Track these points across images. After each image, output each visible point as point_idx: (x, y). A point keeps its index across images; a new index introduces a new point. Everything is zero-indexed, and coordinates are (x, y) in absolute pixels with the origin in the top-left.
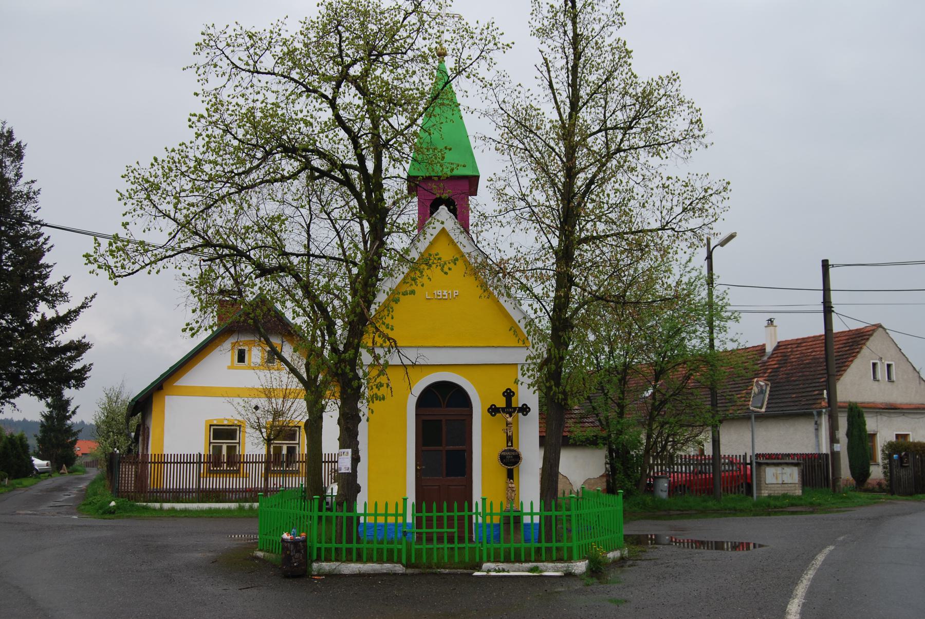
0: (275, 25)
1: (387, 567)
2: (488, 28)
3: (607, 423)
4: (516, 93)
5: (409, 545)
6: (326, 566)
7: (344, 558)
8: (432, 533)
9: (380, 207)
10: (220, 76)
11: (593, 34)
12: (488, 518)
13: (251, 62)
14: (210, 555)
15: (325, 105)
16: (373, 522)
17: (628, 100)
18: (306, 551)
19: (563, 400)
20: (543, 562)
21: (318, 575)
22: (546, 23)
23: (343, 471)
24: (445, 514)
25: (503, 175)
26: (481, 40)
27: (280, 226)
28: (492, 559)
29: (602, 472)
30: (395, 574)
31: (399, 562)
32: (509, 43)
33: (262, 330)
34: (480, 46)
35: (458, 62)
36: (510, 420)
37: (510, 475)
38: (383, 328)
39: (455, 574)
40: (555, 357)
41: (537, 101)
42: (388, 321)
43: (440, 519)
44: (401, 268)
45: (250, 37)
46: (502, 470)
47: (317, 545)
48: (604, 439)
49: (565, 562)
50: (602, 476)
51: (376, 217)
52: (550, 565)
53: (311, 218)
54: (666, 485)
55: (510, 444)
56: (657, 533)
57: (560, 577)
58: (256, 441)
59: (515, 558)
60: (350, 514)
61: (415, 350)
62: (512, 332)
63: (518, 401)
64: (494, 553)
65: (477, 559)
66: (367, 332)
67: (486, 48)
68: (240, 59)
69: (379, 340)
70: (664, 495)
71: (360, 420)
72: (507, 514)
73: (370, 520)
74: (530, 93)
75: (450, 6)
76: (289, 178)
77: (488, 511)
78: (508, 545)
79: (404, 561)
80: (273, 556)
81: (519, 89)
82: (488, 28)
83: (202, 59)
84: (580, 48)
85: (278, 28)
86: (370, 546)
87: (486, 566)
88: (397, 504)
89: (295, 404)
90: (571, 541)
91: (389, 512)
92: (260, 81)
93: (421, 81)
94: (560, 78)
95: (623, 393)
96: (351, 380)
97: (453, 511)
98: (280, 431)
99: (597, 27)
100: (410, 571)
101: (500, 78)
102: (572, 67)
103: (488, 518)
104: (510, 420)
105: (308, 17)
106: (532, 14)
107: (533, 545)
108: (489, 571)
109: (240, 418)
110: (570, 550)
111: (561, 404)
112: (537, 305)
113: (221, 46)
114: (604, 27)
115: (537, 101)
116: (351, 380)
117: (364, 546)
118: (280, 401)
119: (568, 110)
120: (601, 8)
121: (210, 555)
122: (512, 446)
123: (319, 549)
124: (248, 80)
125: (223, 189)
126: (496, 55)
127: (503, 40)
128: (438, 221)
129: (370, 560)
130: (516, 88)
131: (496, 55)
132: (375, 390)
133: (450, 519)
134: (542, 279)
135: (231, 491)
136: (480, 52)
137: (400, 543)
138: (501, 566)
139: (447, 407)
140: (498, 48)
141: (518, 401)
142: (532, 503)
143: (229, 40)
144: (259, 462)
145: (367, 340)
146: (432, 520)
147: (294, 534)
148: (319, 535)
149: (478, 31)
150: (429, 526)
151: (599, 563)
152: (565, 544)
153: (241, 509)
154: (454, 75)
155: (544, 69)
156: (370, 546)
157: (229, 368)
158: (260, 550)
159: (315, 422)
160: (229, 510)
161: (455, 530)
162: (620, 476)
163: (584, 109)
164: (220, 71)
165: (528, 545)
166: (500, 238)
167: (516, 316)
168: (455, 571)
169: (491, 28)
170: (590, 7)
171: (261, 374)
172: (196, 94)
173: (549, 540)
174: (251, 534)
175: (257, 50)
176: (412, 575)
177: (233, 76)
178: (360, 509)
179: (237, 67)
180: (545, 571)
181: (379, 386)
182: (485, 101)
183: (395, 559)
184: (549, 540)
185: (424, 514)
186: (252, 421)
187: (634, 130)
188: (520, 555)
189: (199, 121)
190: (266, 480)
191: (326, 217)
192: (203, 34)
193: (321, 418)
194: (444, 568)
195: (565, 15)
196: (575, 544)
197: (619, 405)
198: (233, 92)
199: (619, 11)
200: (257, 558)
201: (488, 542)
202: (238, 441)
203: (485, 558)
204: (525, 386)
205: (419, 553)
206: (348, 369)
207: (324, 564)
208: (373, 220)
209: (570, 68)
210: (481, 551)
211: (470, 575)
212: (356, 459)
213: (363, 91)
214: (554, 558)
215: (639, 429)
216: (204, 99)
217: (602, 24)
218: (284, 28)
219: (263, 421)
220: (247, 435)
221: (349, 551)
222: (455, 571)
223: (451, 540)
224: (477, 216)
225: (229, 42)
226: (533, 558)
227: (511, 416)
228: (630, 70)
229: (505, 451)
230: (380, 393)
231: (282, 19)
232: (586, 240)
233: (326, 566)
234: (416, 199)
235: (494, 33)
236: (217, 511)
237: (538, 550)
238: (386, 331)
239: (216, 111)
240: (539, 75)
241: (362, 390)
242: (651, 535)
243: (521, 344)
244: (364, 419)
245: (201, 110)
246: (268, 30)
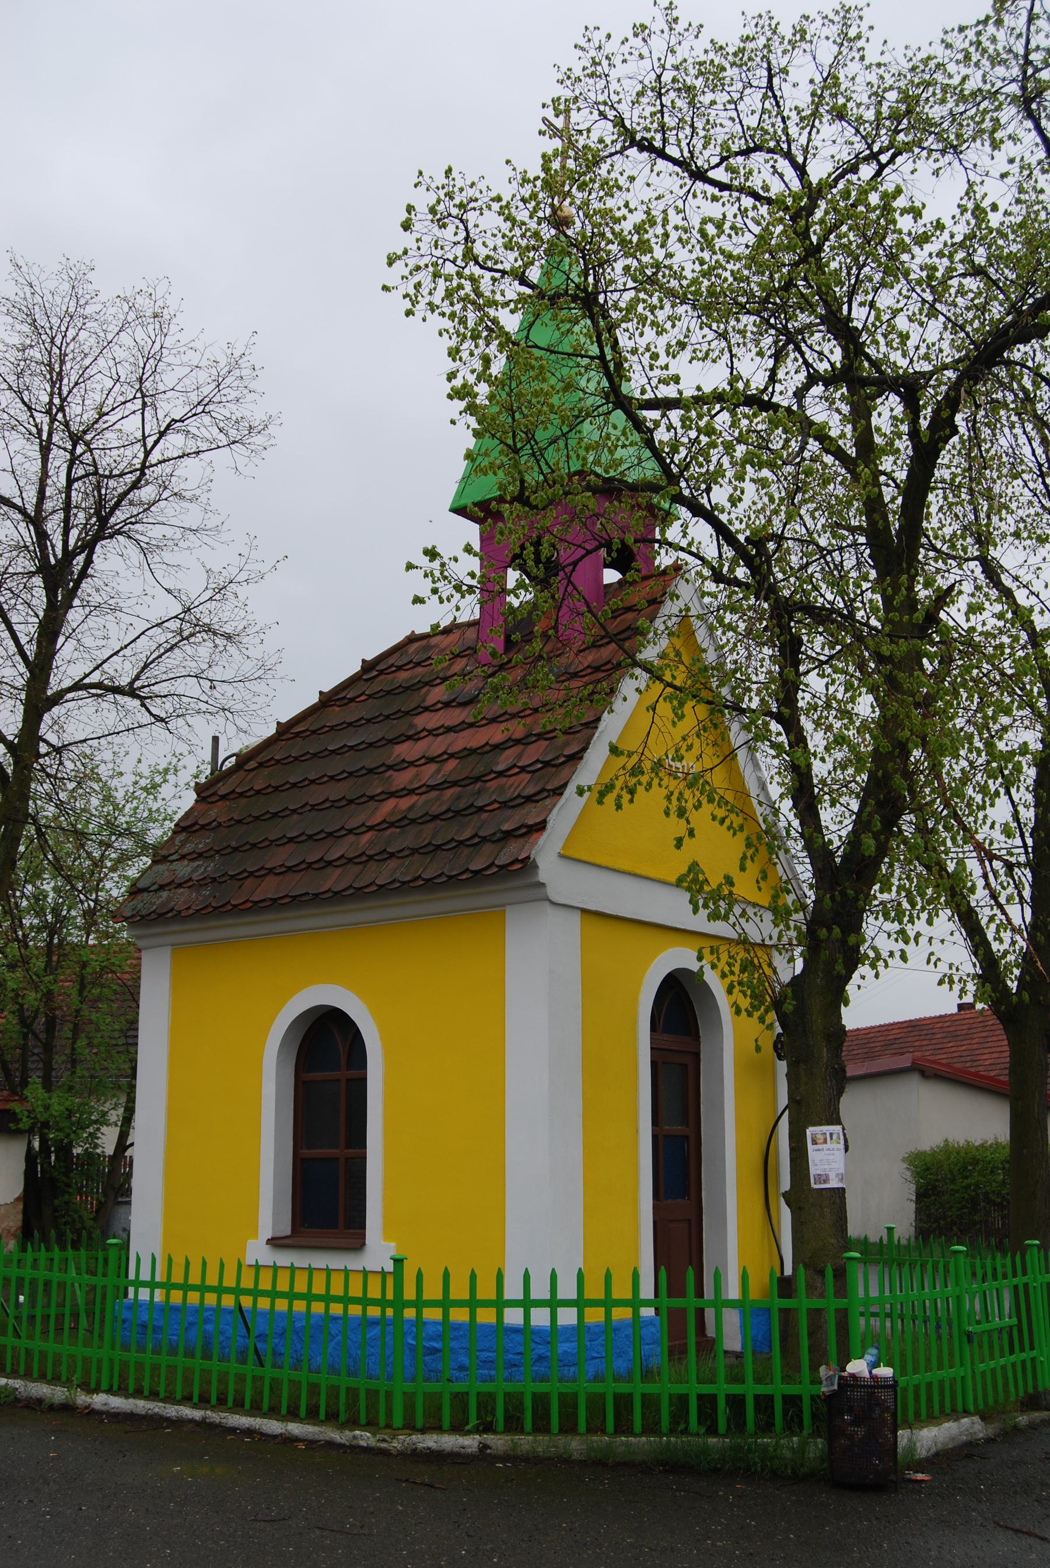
16: (574, 1321)
60: (677, 1303)
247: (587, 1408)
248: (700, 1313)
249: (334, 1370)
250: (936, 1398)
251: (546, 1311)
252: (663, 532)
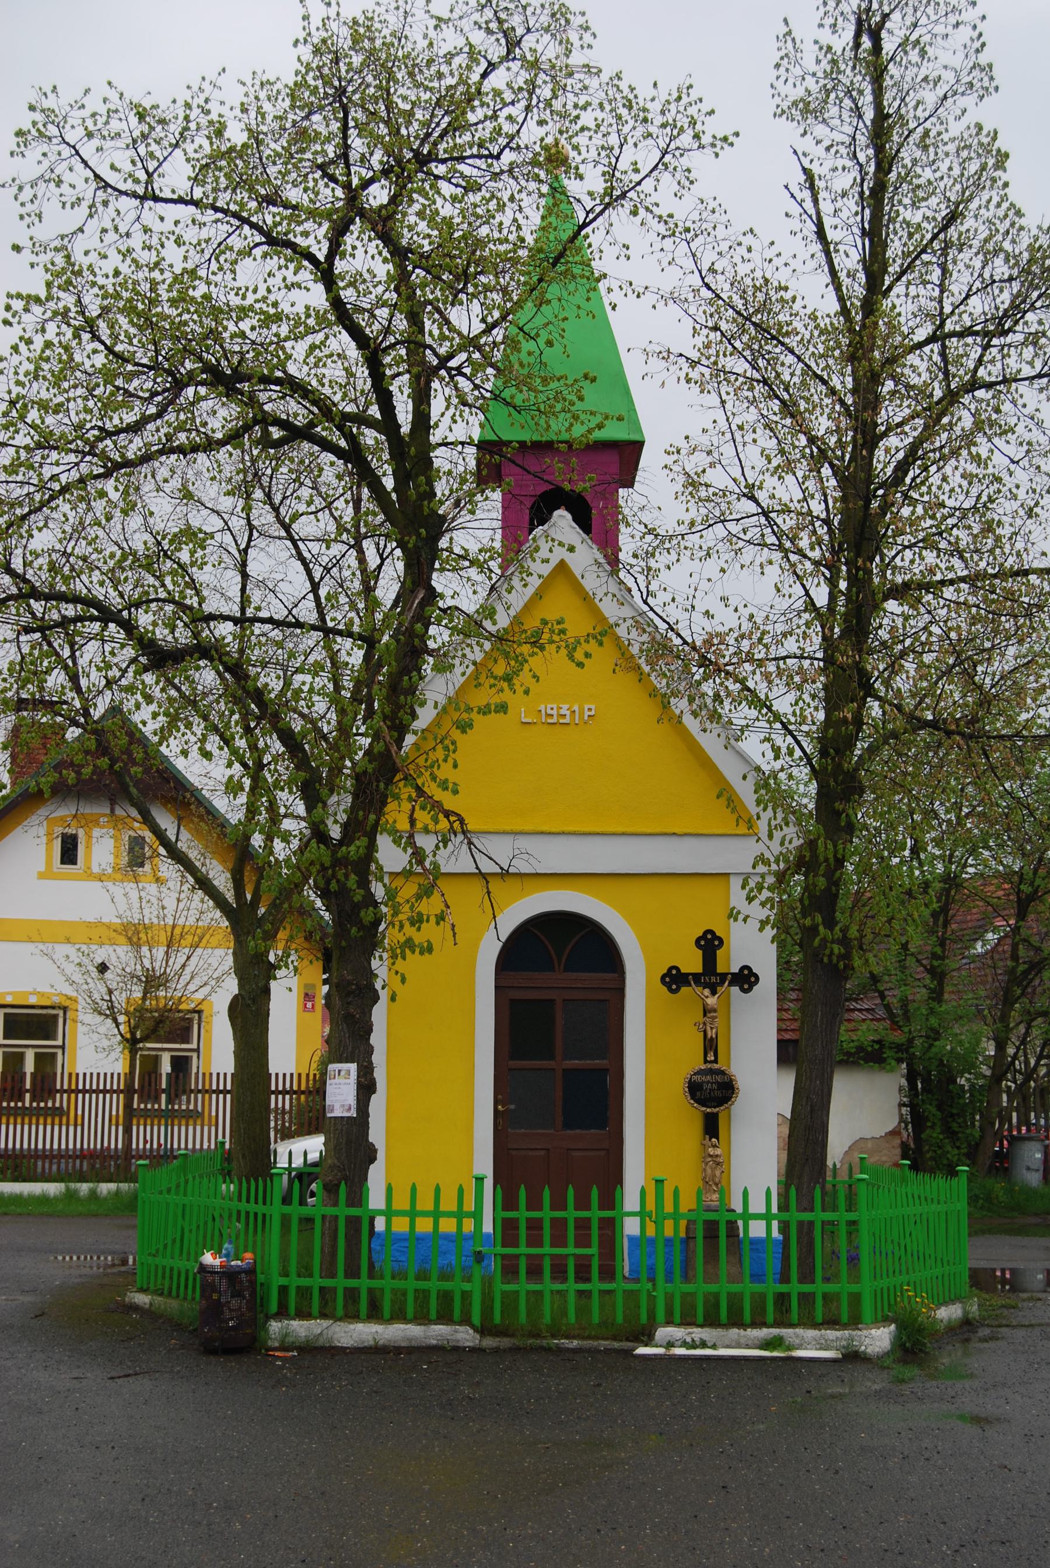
0: (195, 88)
1: (438, 1332)
2: (679, 98)
3: (906, 1012)
4: (742, 251)
5: (487, 1284)
6: (300, 1328)
7: (340, 1312)
8: (541, 1257)
9: (426, 511)
10: (68, 206)
11: (919, 112)
12: (669, 1225)
13: (142, 176)
14: (27, 1299)
15: (306, 275)
16: (763, 1234)
17: (1000, 268)
18: (253, 1293)
19: (841, 957)
20: (791, 1325)
21: (283, 1348)
22: (814, 88)
23: (338, 1113)
24: (571, 1214)
25: (704, 441)
26: (664, 126)
27: (192, 553)
28: (677, 1318)
29: (892, 1123)
30: (456, 1349)
31: (466, 1321)
32: (729, 133)
33: (134, 791)
34: (660, 141)
35: (610, 175)
36: (711, 1001)
37: (711, 1128)
38: (432, 790)
39: (593, 1352)
40: (826, 860)
41: (789, 269)
42: (445, 772)
43: (559, 1225)
44: (467, 651)
45: (141, 117)
46: (692, 1117)
47: (278, 1281)
48: (899, 1048)
49: (845, 1327)
50: (894, 1133)
51: (419, 535)
52: (811, 1333)
53: (251, 535)
54: (1038, 1156)
55: (711, 1057)
56: (1021, 1266)
58: (105, 1043)
59: (728, 1318)
60: (354, 1211)
61: (508, 840)
62: (723, 800)
63: (731, 960)
64: (682, 1304)
65: (644, 1319)
66: (397, 797)
67: (673, 146)
68: (113, 167)
69: (423, 817)
70: (1034, 1179)
71: (376, 998)
72: (711, 1216)
73: (401, 1225)
74: (774, 250)
75: (590, 46)
76: (222, 443)
77: (669, 1208)
78: (712, 1288)
79: (476, 1319)
80: (174, 1304)
81: (748, 240)
82: (679, 98)
83: (29, 167)
84: (890, 147)
85: (202, 97)
86: (399, 1284)
87: (663, 1333)
88: (461, 1190)
89: (194, 960)
91: (419, 1208)
92: (162, 219)
93: (515, 220)
94: (844, 214)
95: (942, 943)
96: (357, 907)
97: (540, 1208)
98: (159, 1022)
99: (931, 97)
100: (489, 1342)
101: (704, 215)
102: (871, 190)
103: (669, 1225)
104: (711, 1001)
105: (259, 72)
106: (777, 66)
107: (771, 1288)
108: (670, 1345)
109: (70, 991)
110: (855, 1300)
111: (836, 965)
112: (783, 742)
113: (71, 137)
114: (945, 97)
115: (789, 269)
116: (357, 907)
117: (387, 1284)
118: (160, 953)
119: (860, 291)
120: (939, 53)
121: (27, 1299)
122: (716, 1061)
123: (283, 1290)
124: (132, 216)
125: (83, 465)
126: (698, 161)
127: (712, 128)
128: (561, 544)
129: (399, 1316)
130: (741, 238)
131: (698, 161)
132: (409, 931)
133: (583, 1225)
134: (795, 682)
135: (36, 1155)
136: (659, 155)
137: (468, 1279)
138: (698, 1333)
139: (566, 970)
140: (701, 147)
141: (731, 960)
143: (89, 123)
144: (112, 1091)
145: (397, 813)
146: (541, 1228)
147: (227, 1256)
148: (284, 1259)
149: (655, 107)
150: (535, 1240)
151: (920, 1330)
152: (843, 1287)
153: (70, 1196)
154: (598, 209)
155: (807, 194)
156: (399, 1284)
157: (42, 876)
158: (142, 1290)
159: (254, 1000)
160: (44, 1199)
161: (594, 1250)
162: (934, 1134)
163: (899, 289)
164: (70, 195)
165: (758, 1288)
166: (704, 585)
167: (731, 770)
168: (594, 1343)
169: (685, 100)
170: (917, 50)
171: (117, 890)
172: (17, 248)
173: (806, 1276)
174: (103, 1253)
175: (154, 147)
176: (496, 1351)
177: (101, 208)
178: (376, 1199)
179: (107, 185)
180: (799, 1347)
181: (417, 921)
182: (668, 269)
183: (457, 1315)
184: (806, 1276)
185: (523, 1214)
186: (96, 996)
187: (1010, 338)
188: (741, 1310)
189: (27, 310)
190: (128, 1131)
191: (283, 534)
192: (32, 108)
193: (267, 991)
194: (567, 1337)
195: (854, 68)
196: (866, 1287)
197: (932, 971)
198: (98, 245)
199: (983, 59)
200: (135, 1308)
201: (669, 1278)
202: (59, 1042)
203: (661, 1315)
204: (754, 924)
205: (510, 1301)
206: (352, 881)
207: (295, 1324)
208: (412, 541)
209: (867, 193)
210: (652, 1299)
211: (628, 1353)
212: (366, 1088)
213: (388, 238)
214: (819, 1318)
215: (977, 1026)
216: (34, 259)
217: (940, 91)
218: (216, 95)
219: (120, 999)
220: (81, 1029)
221: (352, 1295)
222: (594, 1343)
223: (583, 1273)
224: (638, 535)
225: (91, 128)
226: (770, 1318)
227: (714, 993)
228: (1004, 198)
229: (700, 1072)
230: (419, 938)
231: (211, 76)
232: (899, 592)
233: (300, 1328)
234: (497, 496)
235: (692, 111)
236: (17, 1199)
237: (782, 1299)
238: (438, 794)
239: (67, 286)
240: (796, 210)
241: (381, 928)
242: (1003, 1271)
243: (743, 829)
244: (384, 995)
245: (35, 284)
246: (180, 102)
249: (423, 1275)
251: (406, 1220)
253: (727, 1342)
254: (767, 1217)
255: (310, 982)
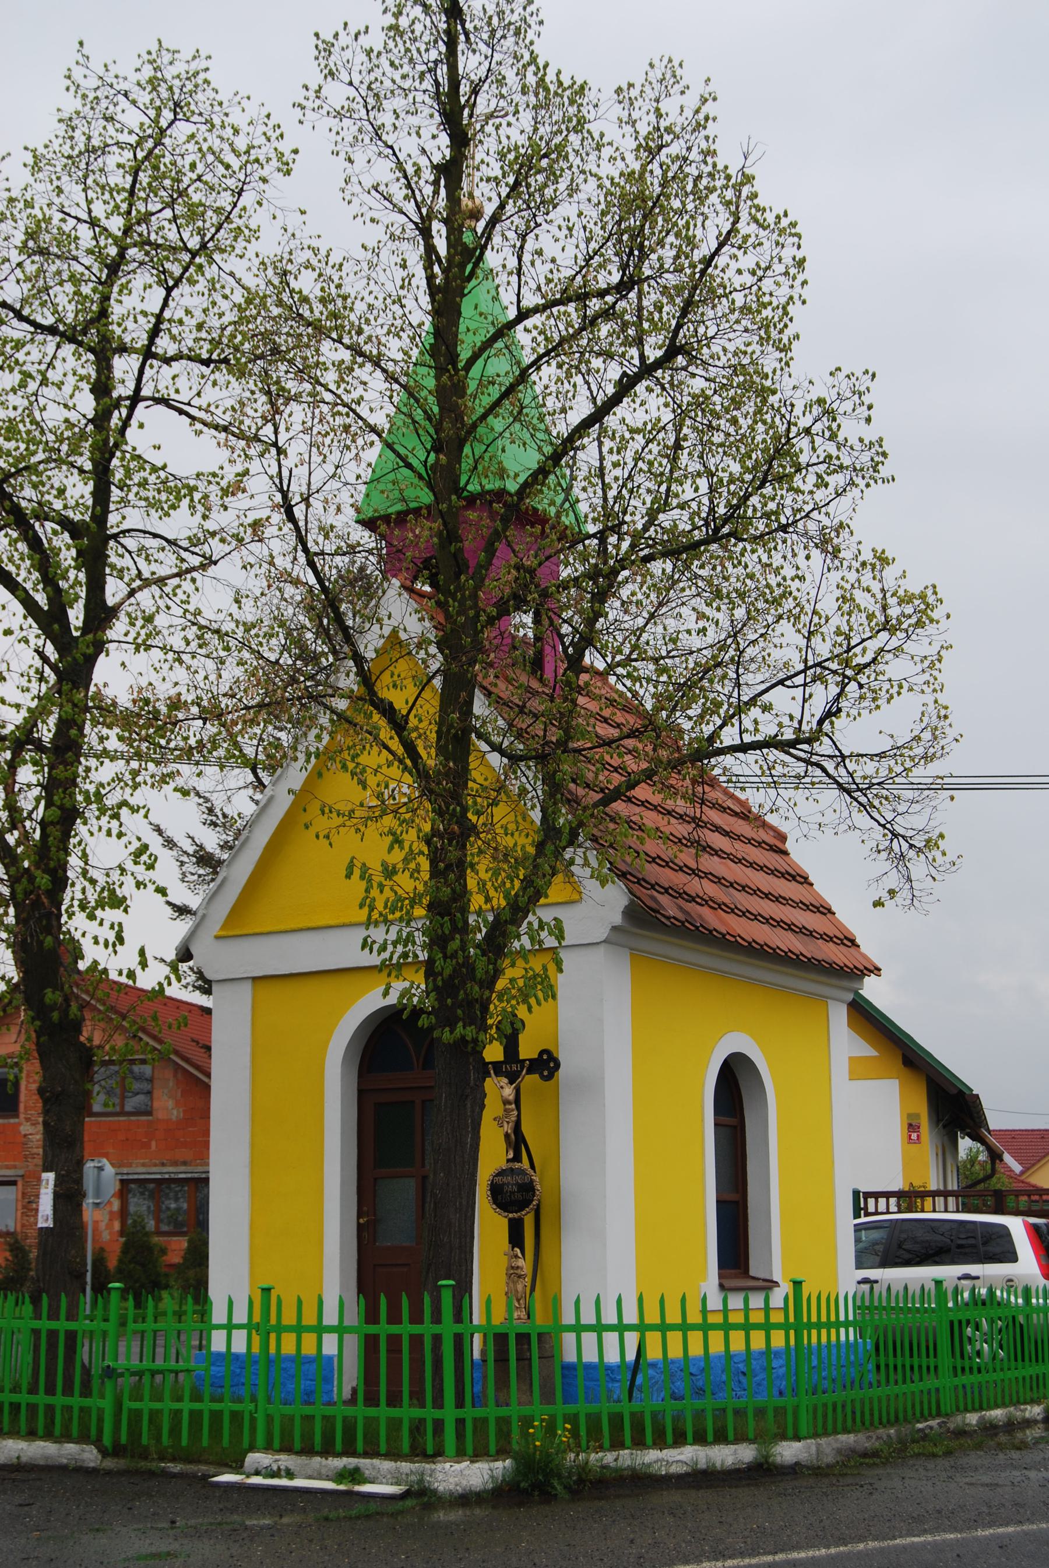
1: (69, 1451)
52: (386, 1465)
57: (391, 1498)
60: (372, 1329)
87: (256, 1459)
90: (441, 1407)
100: (109, 1464)
138: (285, 1460)
142: (231, 1303)
200: (1033, 1402)
247: (632, 1426)
248: (458, 1339)
250: (926, 1407)
252: (511, 495)
253: (310, 1473)
254: (340, 1330)
255: (912, 1111)
